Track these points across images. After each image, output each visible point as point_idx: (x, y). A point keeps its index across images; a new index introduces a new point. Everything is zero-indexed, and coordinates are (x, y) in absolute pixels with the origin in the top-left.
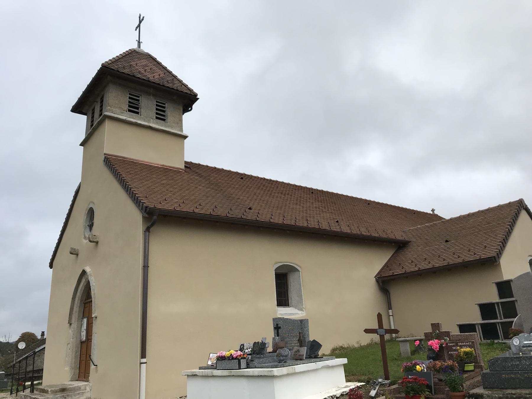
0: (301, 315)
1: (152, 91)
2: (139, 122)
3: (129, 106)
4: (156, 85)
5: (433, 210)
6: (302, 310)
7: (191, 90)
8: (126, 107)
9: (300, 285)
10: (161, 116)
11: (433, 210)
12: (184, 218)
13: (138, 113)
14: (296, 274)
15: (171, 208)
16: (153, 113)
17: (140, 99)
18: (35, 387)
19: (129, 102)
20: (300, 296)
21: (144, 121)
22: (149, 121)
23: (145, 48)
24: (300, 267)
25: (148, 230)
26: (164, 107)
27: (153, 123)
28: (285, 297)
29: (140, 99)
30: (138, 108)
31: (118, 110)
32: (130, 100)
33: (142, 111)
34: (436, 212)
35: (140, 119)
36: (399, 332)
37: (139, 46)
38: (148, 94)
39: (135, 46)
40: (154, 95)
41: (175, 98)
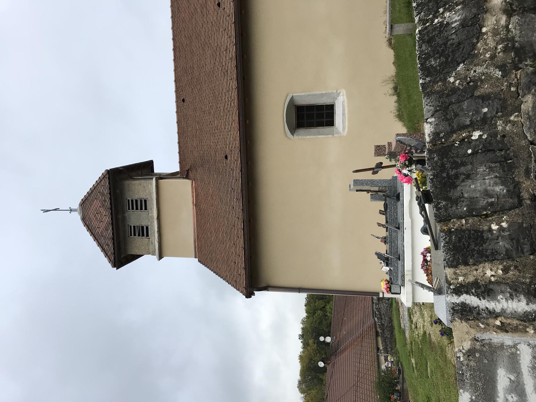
0: (345, 97)
1: (120, 216)
2: (156, 229)
3: (143, 235)
6: (339, 94)
8: (145, 239)
9: (309, 95)
10: (143, 205)
12: (242, 35)
13: (147, 228)
15: (233, 26)
16: (143, 213)
17: (130, 199)
18: (393, 150)
19: (139, 235)
20: (322, 95)
21: (153, 222)
22: (152, 217)
23: (76, 205)
24: (288, 95)
25: (266, 288)
26: (132, 201)
27: (152, 213)
29: (130, 199)
30: (143, 227)
31: (151, 247)
32: (137, 234)
33: (144, 223)
35: (153, 226)
37: (75, 210)
38: (124, 219)
39: (77, 217)
40: (124, 212)
41: (120, 216)
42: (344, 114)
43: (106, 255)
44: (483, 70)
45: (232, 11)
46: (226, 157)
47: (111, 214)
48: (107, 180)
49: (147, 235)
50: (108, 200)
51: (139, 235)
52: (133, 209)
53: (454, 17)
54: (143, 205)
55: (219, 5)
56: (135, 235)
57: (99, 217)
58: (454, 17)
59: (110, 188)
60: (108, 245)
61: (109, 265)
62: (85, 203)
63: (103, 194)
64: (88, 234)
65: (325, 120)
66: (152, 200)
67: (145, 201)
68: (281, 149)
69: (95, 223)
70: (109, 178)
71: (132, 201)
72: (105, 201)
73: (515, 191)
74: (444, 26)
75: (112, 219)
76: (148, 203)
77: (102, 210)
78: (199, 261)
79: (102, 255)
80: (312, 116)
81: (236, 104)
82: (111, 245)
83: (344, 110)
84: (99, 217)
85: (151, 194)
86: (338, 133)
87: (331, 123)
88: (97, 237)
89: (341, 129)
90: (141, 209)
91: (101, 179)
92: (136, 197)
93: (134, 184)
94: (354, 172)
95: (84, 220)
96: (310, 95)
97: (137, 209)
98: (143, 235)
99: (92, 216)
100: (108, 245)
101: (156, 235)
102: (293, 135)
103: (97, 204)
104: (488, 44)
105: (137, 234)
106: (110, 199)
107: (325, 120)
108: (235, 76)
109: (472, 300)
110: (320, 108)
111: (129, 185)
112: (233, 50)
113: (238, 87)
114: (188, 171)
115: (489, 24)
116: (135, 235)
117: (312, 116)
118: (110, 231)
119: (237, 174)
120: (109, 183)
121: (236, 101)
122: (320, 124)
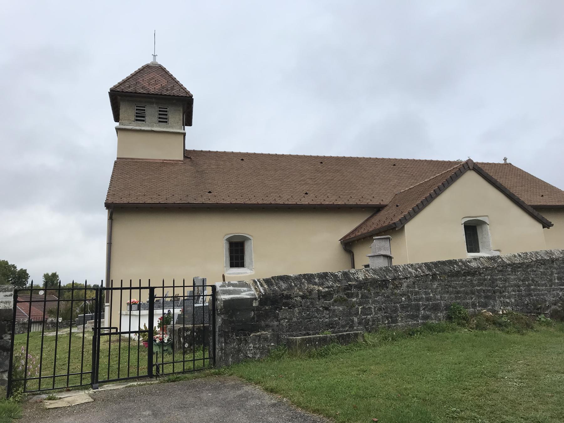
2: (143, 128)
3: (137, 116)
4: (156, 96)
5: (505, 159)
6: (251, 270)
7: (188, 92)
8: (133, 118)
10: (163, 120)
11: (505, 159)
13: (144, 121)
14: (249, 242)
16: (156, 119)
19: (136, 113)
21: (149, 126)
22: (152, 126)
23: (160, 61)
25: (111, 218)
26: (167, 111)
27: (156, 126)
28: (241, 260)
30: (144, 117)
31: (127, 122)
32: (137, 111)
33: (147, 119)
34: (508, 162)
35: (145, 126)
36: (45, 275)
37: (155, 59)
38: (152, 103)
39: (149, 60)
40: (157, 103)
42: (239, 273)
43: (120, 84)
44: (306, 286)
45: (303, 203)
46: (210, 192)
47: (157, 94)
48: (184, 95)
49: (137, 120)
50: (168, 93)
51: (136, 113)
52: (159, 111)
53: (317, 280)
54: (163, 120)
55: (306, 194)
56: (137, 110)
57: (152, 82)
58: (317, 280)
59: (178, 96)
60: (129, 87)
61: (112, 86)
62: (161, 69)
63: (172, 88)
64: (136, 69)
65: (234, 261)
66: (167, 127)
67: (166, 122)
68: (215, 233)
69: (147, 77)
70: (186, 97)
71: (167, 111)
72: (167, 90)
73: (283, 290)
74: (315, 279)
75: (153, 94)
76: (165, 124)
77: (158, 87)
78: (116, 162)
79: (120, 80)
80: (237, 253)
81: (247, 202)
82: (129, 90)
83: (241, 273)
84: (152, 82)
85: (172, 127)
86: (227, 270)
87: (232, 265)
88: (134, 77)
89: (229, 272)
90: (159, 118)
91: (184, 89)
92: (170, 115)
93: (180, 115)
94: (224, 276)
95: (147, 67)
96: (251, 252)
97: (159, 114)
98: (137, 116)
99: (152, 75)
100: (129, 87)
101: (138, 128)
102: (226, 240)
103: (164, 82)
104: (312, 286)
105: (137, 111)
106: (170, 95)
107: (234, 261)
108: (265, 202)
109: (258, 283)
110: (242, 258)
111: (180, 110)
112: (280, 202)
113: (258, 204)
114: (190, 158)
115: (316, 287)
116: (137, 110)
117: (237, 253)
118: (142, 91)
119: (200, 200)
120: (182, 96)
121: (249, 202)
122: (231, 258)
